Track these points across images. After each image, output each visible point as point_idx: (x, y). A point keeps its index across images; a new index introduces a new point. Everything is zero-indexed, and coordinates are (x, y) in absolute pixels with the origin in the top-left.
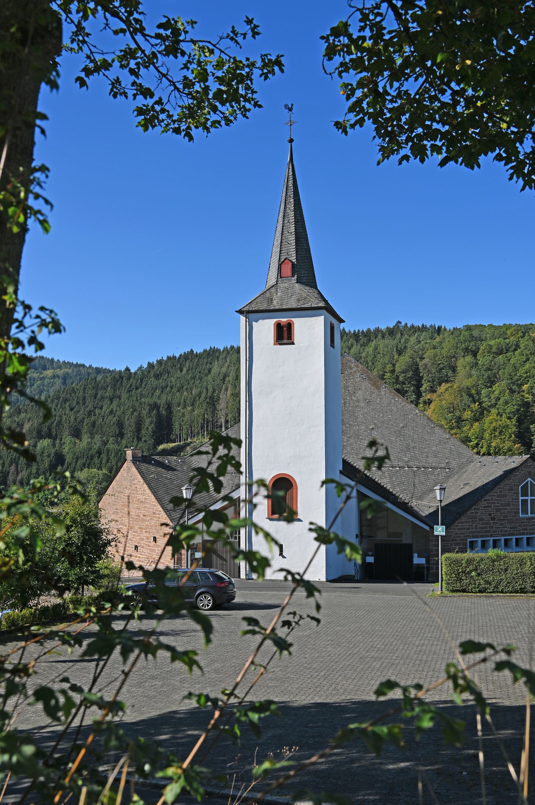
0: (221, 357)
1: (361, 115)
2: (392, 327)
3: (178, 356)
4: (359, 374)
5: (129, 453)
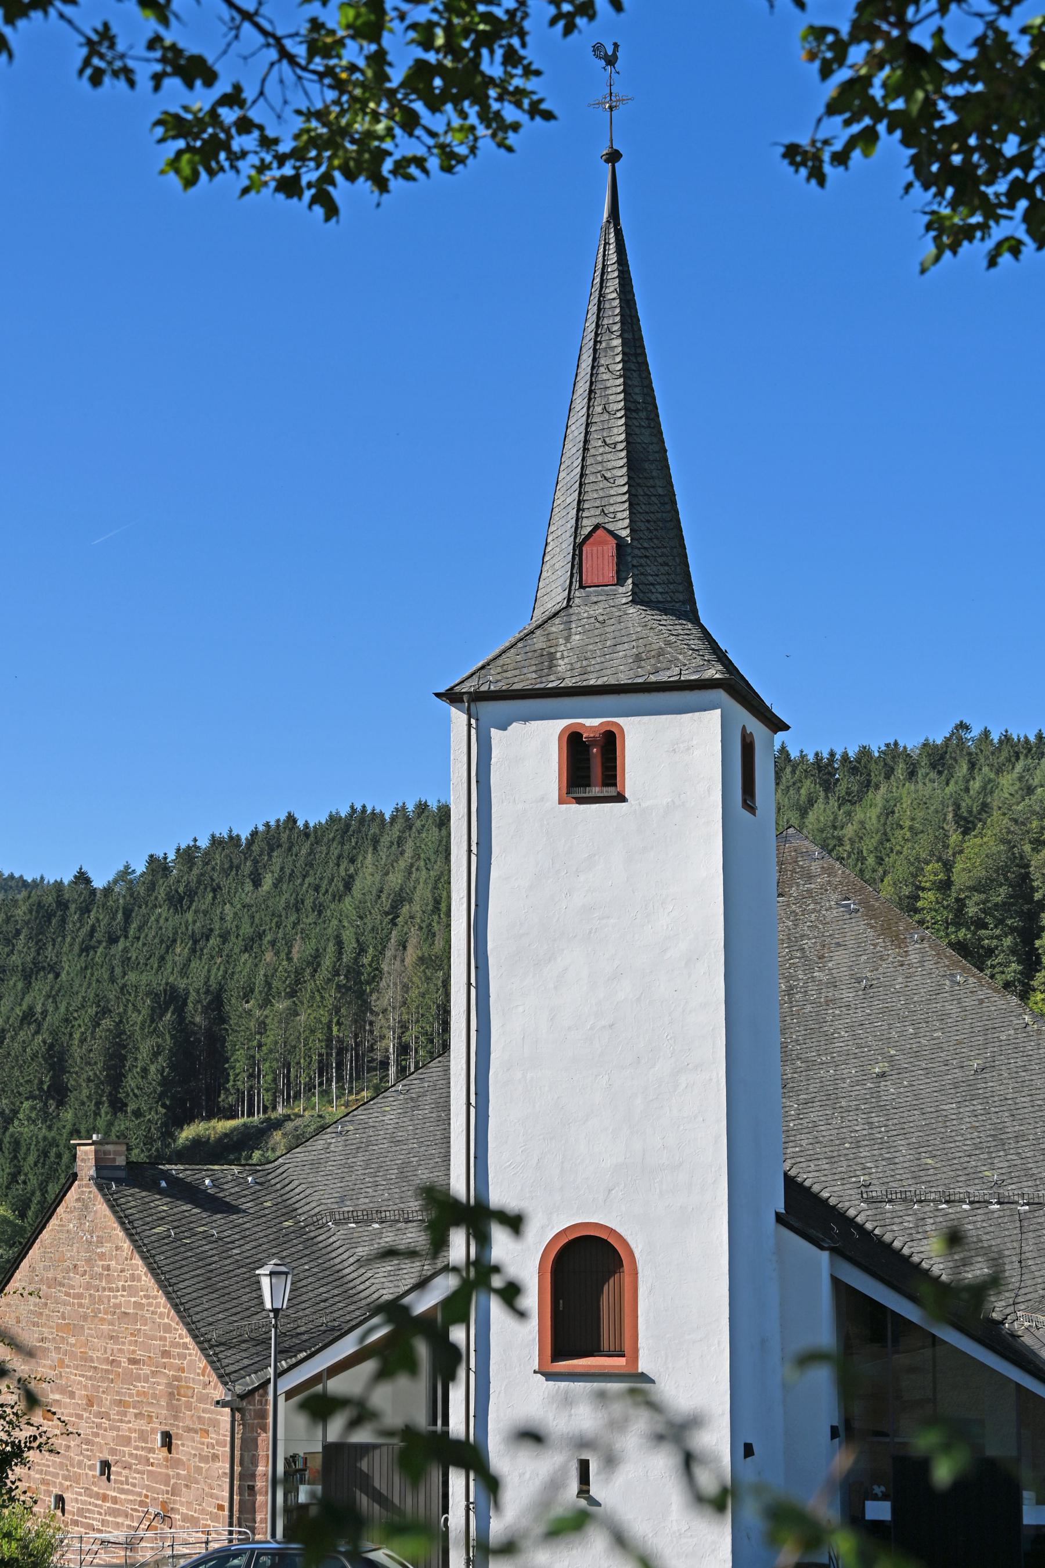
0: (385, 840)
1: (867, 121)
2: (939, 741)
3: (245, 835)
4: (834, 897)
5: (86, 1154)
